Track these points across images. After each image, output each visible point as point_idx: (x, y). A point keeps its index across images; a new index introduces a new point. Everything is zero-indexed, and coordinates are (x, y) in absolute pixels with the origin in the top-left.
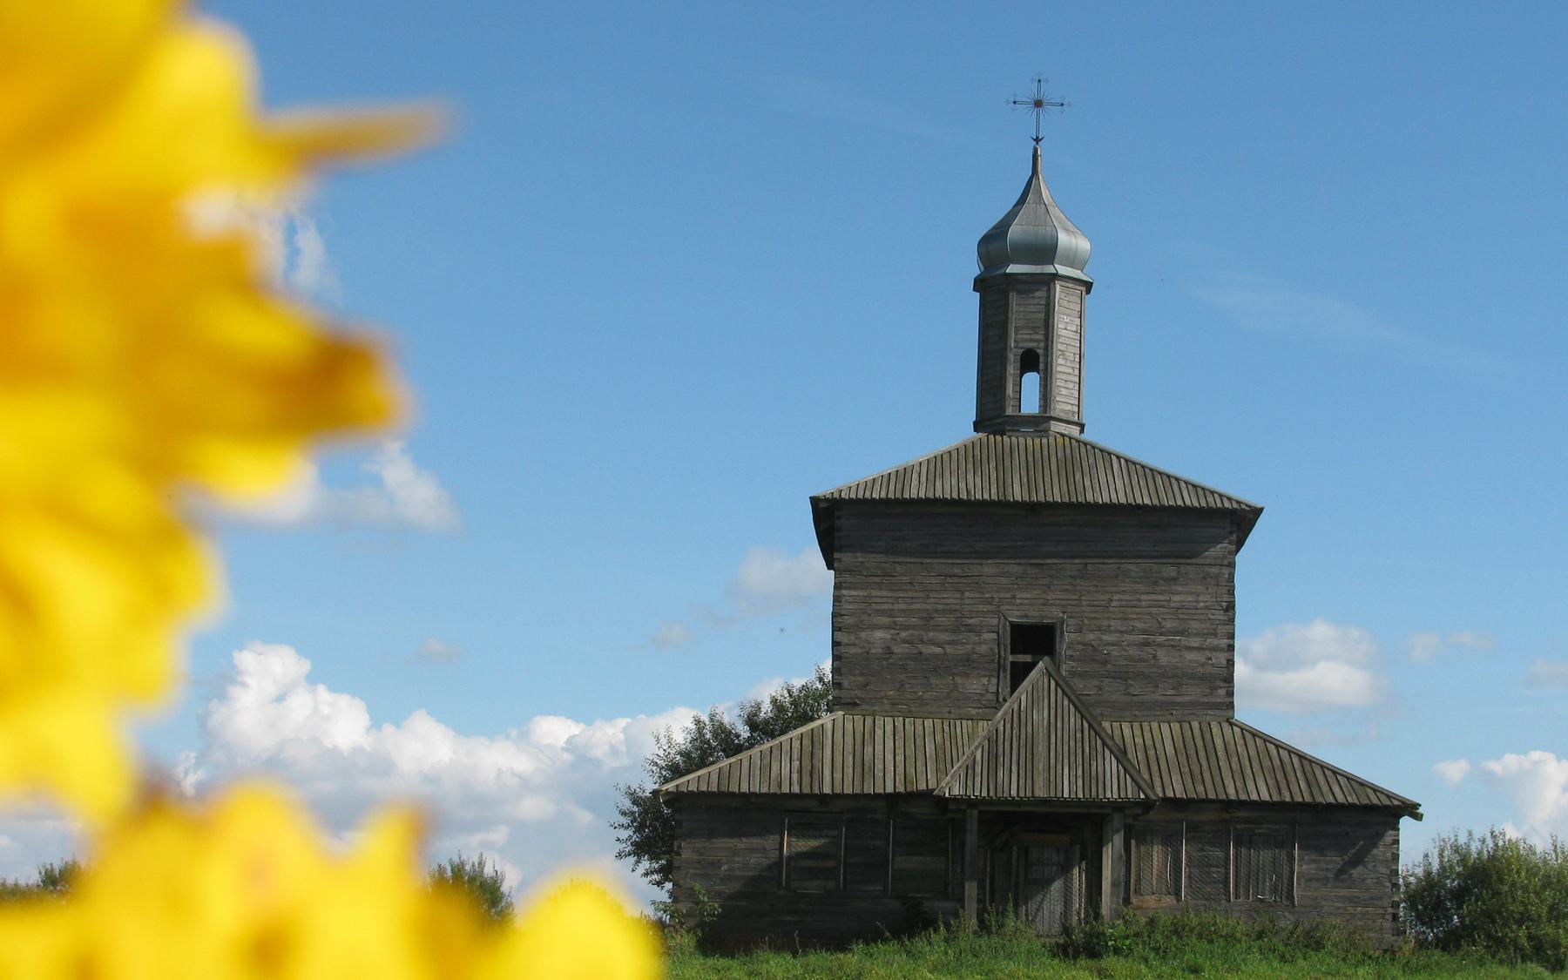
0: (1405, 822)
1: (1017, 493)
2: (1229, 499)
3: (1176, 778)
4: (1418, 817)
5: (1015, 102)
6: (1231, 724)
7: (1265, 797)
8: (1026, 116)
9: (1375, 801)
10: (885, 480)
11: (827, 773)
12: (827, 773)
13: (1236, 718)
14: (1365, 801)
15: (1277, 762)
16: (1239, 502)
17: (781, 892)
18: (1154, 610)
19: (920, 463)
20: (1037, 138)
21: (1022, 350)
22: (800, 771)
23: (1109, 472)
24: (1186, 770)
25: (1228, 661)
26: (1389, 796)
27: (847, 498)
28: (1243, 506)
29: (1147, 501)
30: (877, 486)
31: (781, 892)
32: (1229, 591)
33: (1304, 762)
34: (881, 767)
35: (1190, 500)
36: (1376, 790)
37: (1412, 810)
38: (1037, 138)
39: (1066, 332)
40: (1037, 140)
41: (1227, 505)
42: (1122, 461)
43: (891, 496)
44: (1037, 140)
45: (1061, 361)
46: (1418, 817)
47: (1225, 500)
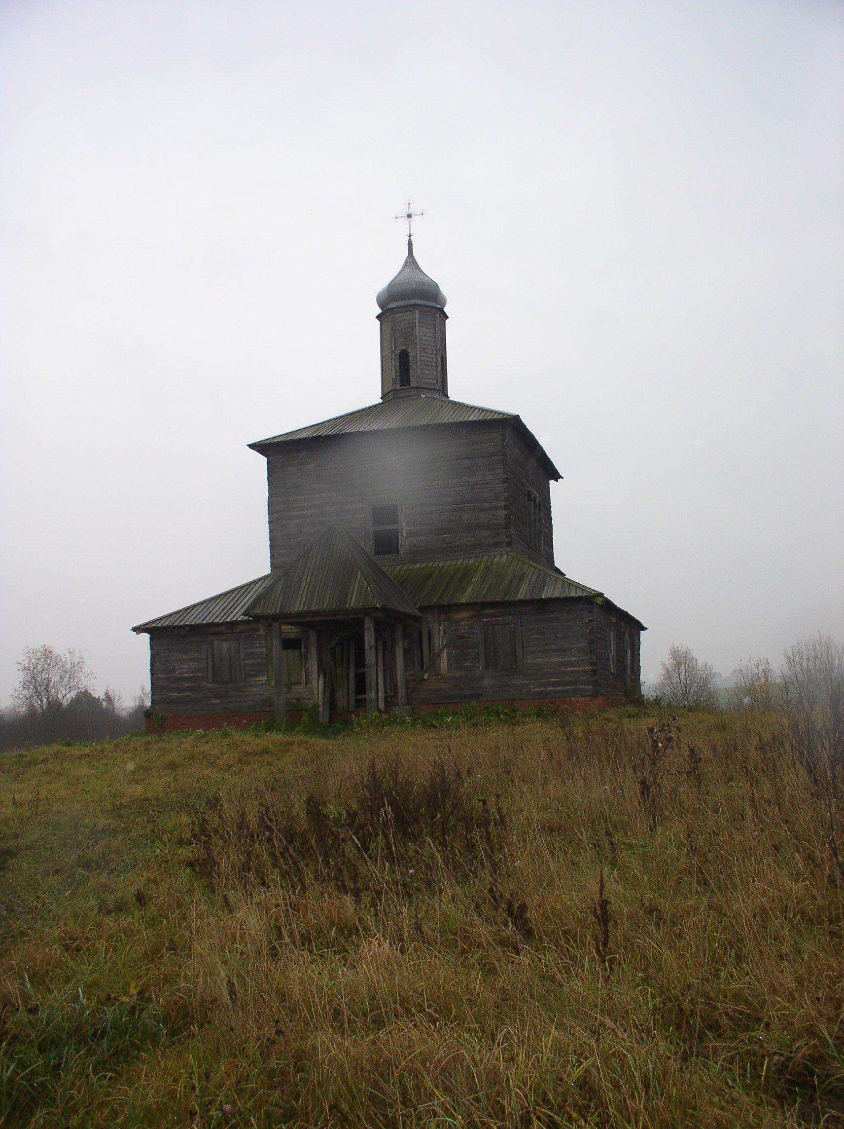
40: (410, 236)
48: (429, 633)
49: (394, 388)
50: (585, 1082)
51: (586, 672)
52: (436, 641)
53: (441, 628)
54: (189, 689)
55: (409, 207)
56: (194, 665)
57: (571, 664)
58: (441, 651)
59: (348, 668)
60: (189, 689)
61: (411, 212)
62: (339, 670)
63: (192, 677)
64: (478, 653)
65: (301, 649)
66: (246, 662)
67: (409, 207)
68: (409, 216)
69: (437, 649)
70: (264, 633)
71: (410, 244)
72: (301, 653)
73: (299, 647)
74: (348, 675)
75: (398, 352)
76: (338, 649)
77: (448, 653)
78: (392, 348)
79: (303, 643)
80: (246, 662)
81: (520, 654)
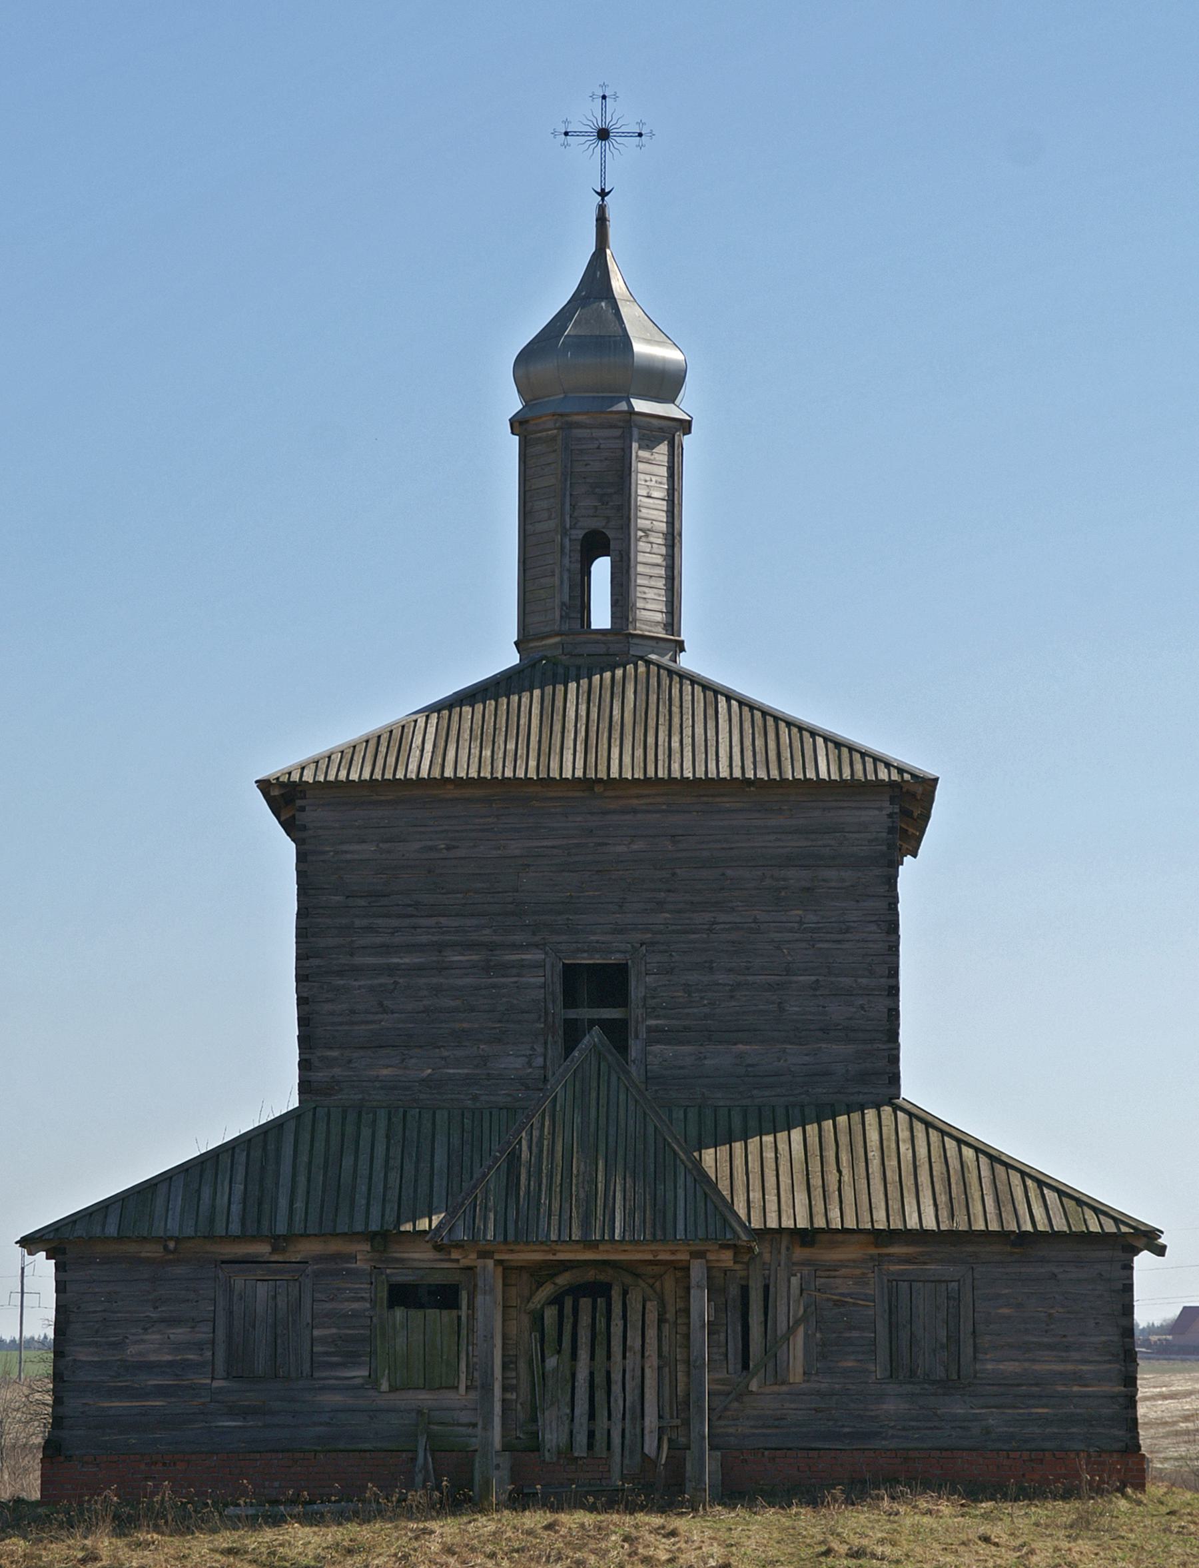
0: (1143, 1261)
1: (571, 766)
2: (888, 765)
3: (801, 1197)
4: (1160, 1251)
5: (566, 134)
6: (896, 1108)
7: (930, 1224)
8: (585, 151)
9: (1094, 1227)
10: (372, 744)
11: (283, 1202)
12: (283, 1202)
13: (902, 1095)
14: (1078, 1227)
15: (954, 1163)
16: (901, 771)
17: (216, 1384)
18: (468, 1081)
19: (403, 727)
20: (603, 190)
21: (584, 532)
22: (244, 1201)
23: (711, 724)
24: (816, 1181)
25: (890, 1010)
26: (1118, 1219)
27: (311, 781)
28: (907, 777)
29: (762, 774)
30: (323, 766)
31: (216, 1384)
32: (890, 904)
33: (998, 1167)
34: (364, 1188)
35: (825, 768)
36: (1099, 1210)
37: (1150, 1239)
38: (603, 190)
39: (651, 501)
40: (603, 194)
41: (883, 774)
42: (734, 703)
43: (378, 776)
44: (603, 194)
45: (642, 545)
46: (1160, 1251)
47: (881, 767)
48: (766, 1288)
49: (565, 627)
50: (1124, 1314)
51: (1113, 1397)
52: (782, 1309)
53: (795, 1281)
54: (161, 1391)
55: (604, 109)
56: (179, 1333)
57: (1078, 1378)
58: (791, 1330)
59: (574, 1356)
60: (161, 1391)
61: (615, 141)
62: (551, 1362)
63: (171, 1364)
64: (874, 1342)
65: (457, 1306)
66: (316, 1333)
67: (604, 109)
68: (603, 134)
69: (782, 1327)
70: (367, 1267)
71: (602, 221)
72: (459, 1318)
73: (454, 1305)
74: (573, 1375)
75: (579, 534)
76: (550, 1314)
77: (806, 1335)
78: (563, 521)
79: (464, 1295)
80: (316, 1333)
81: (967, 1351)
